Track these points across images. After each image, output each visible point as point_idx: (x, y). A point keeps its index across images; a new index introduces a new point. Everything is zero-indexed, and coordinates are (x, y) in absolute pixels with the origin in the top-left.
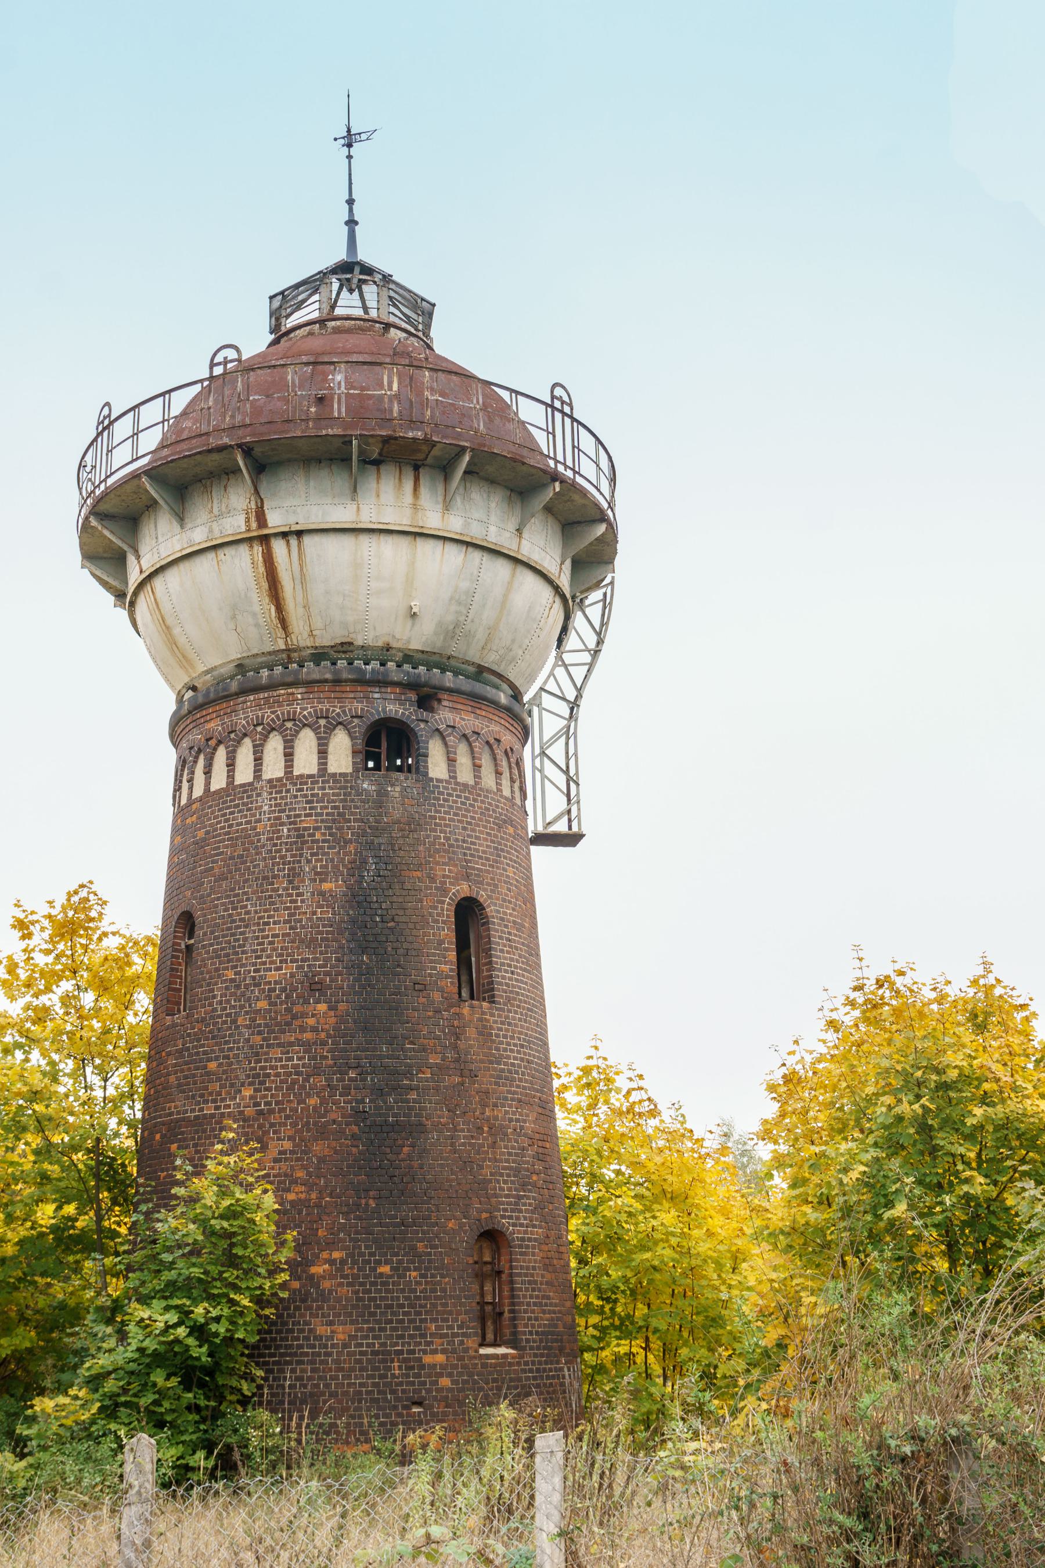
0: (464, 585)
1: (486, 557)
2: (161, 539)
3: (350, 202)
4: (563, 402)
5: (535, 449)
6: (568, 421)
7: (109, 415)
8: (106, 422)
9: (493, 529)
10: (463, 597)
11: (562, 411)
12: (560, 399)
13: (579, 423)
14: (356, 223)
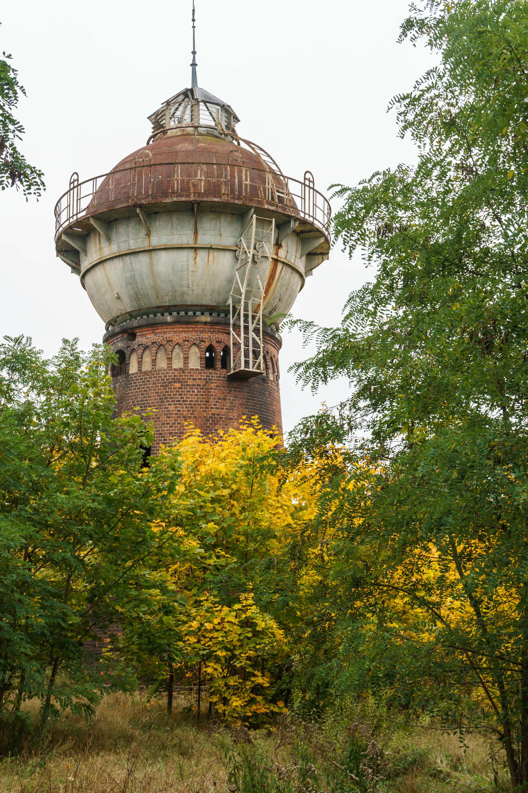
0: (128, 275)
1: (133, 258)
2: (95, 251)
3: (194, 53)
4: (310, 181)
5: (295, 207)
6: (311, 191)
7: (78, 180)
8: (76, 184)
9: (132, 242)
10: (131, 281)
11: (309, 186)
12: (309, 180)
13: (317, 192)
14: (196, 65)
